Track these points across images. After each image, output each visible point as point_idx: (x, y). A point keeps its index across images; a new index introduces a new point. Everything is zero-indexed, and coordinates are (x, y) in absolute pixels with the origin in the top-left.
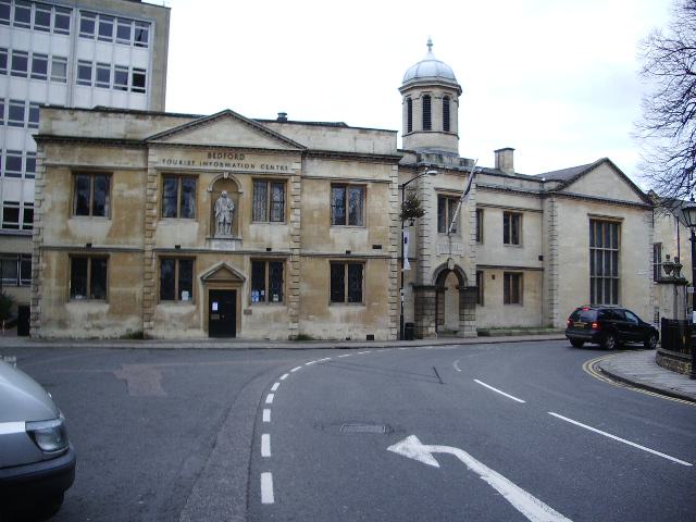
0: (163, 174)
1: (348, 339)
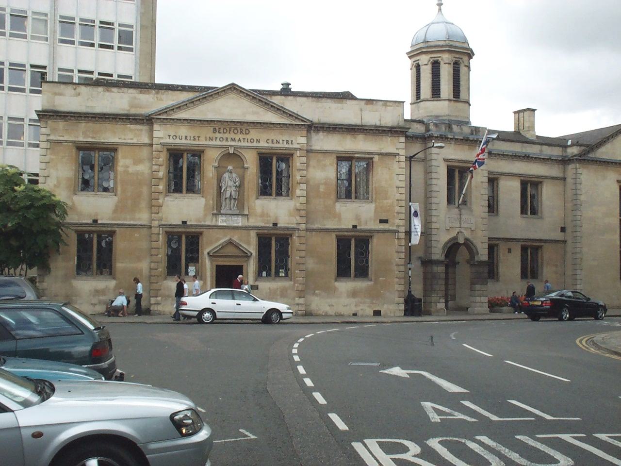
0: (168, 150)
1: (355, 315)
